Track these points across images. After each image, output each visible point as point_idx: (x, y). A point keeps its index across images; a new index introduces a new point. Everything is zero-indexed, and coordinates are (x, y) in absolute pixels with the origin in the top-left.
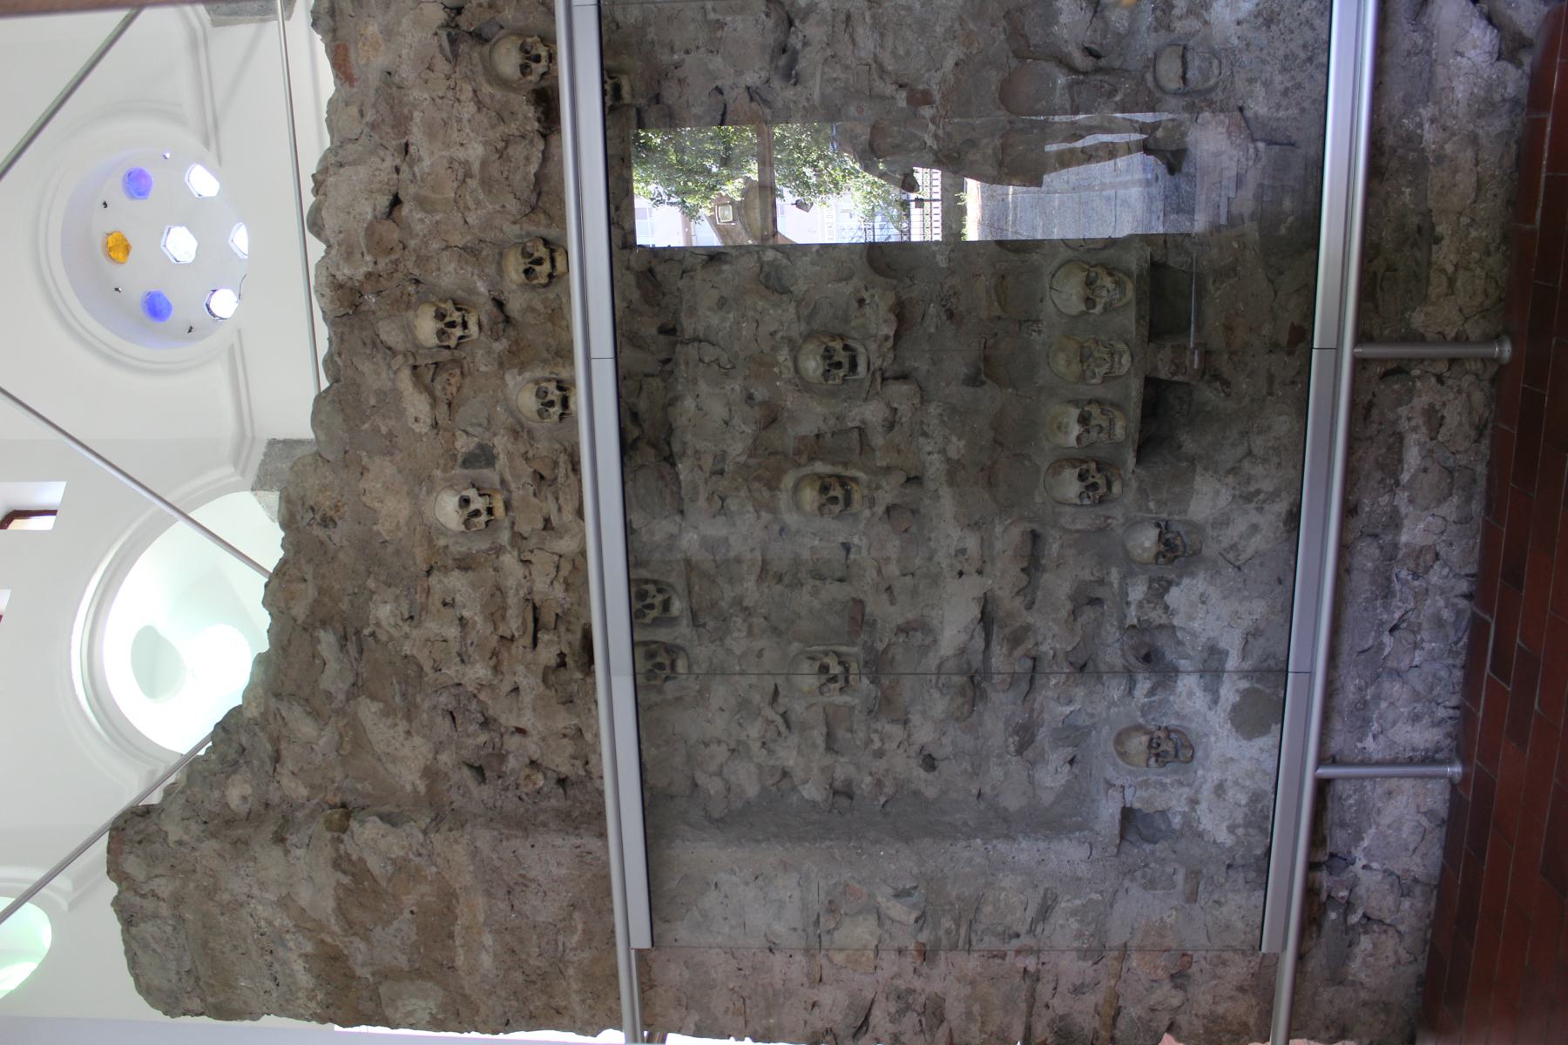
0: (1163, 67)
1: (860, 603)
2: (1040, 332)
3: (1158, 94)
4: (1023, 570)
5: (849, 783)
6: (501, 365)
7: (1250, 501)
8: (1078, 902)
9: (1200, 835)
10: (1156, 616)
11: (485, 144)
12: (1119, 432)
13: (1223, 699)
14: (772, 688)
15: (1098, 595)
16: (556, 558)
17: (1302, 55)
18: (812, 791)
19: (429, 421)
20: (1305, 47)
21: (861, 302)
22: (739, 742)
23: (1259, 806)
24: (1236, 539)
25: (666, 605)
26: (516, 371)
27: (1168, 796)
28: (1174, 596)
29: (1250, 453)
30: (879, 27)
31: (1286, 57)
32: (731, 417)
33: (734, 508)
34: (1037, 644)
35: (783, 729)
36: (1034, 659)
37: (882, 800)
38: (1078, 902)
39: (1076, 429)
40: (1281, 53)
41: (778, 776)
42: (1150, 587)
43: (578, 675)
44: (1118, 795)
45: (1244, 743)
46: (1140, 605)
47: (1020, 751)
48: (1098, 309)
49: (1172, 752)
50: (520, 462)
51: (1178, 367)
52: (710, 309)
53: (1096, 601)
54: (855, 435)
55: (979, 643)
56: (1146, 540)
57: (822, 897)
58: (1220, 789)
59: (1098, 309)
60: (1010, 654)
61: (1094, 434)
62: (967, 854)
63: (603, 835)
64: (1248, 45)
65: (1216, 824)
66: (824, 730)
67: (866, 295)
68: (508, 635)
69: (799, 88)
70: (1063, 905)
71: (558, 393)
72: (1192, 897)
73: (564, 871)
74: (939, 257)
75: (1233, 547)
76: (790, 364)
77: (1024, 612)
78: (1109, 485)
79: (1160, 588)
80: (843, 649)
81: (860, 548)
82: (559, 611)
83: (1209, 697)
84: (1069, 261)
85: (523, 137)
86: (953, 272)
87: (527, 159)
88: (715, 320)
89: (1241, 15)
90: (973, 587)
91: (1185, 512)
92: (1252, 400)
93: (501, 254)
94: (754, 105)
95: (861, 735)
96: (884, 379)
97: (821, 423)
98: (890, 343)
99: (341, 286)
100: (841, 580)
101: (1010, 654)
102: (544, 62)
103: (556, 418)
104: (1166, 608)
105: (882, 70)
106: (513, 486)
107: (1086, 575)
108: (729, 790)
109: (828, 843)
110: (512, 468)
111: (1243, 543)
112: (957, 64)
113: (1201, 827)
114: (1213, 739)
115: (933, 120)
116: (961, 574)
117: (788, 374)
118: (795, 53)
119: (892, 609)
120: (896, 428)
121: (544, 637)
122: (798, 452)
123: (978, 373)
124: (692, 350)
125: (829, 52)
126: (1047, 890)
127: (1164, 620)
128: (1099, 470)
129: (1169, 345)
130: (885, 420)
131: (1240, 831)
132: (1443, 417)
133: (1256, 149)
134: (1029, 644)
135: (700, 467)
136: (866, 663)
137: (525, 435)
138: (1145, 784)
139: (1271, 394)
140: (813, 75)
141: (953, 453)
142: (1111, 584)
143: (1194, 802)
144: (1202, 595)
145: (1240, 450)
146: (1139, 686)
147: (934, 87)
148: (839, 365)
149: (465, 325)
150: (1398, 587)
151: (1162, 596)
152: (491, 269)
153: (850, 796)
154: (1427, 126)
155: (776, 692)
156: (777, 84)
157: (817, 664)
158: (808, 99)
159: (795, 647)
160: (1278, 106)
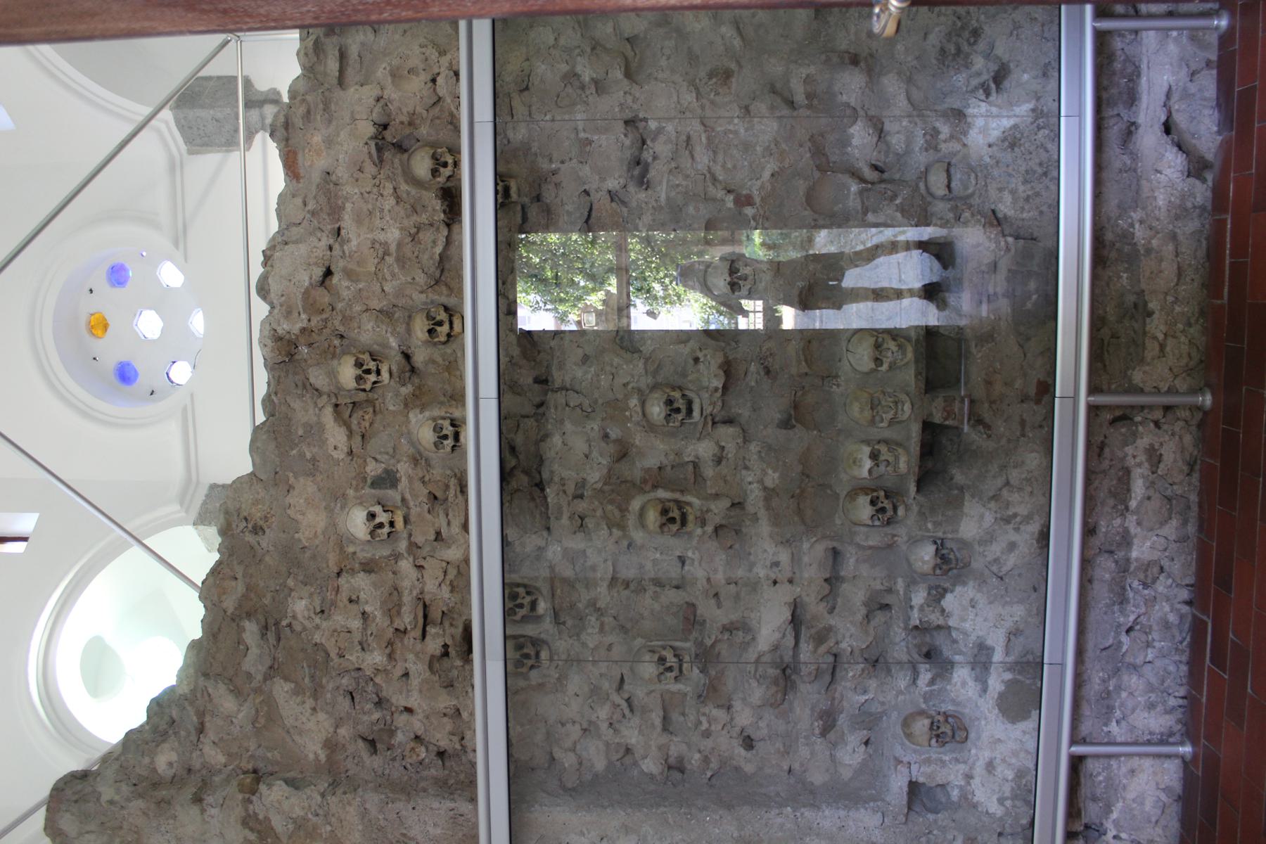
1: (692, 606)
2: (838, 386)
3: (929, 199)
5: (681, 759)
6: (406, 405)
10: (935, 618)
11: (401, 229)
13: (990, 688)
16: (444, 564)
17: (1040, 171)
18: (650, 765)
19: (346, 449)
20: (1041, 164)
21: (696, 360)
22: (590, 722)
24: (998, 554)
25: (533, 605)
26: (418, 411)
27: (947, 771)
28: (949, 601)
29: (1007, 483)
30: (712, 146)
31: (1027, 172)
32: (591, 452)
34: (837, 643)
35: (627, 712)
36: (835, 655)
37: (709, 774)
39: (868, 464)
40: (1023, 169)
41: (622, 751)
42: (929, 594)
43: (458, 663)
45: (1009, 726)
46: (921, 609)
48: (885, 367)
49: (950, 733)
52: (576, 364)
53: (886, 607)
54: (690, 468)
55: (790, 641)
58: (990, 767)
59: (885, 367)
60: (815, 651)
64: (997, 162)
66: (661, 713)
67: (700, 355)
68: (402, 628)
69: (650, 192)
73: (439, 831)
75: (996, 560)
76: (639, 409)
79: (937, 595)
82: (445, 609)
85: (431, 225)
87: (434, 242)
89: (991, 140)
90: (785, 594)
91: (957, 531)
92: (1009, 441)
93: (410, 317)
94: (614, 205)
95: (692, 718)
96: (714, 423)
97: (663, 458)
99: (280, 339)
101: (815, 651)
102: (450, 168)
103: (449, 449)
104: (943, 611)
105: (715, 180)
106: (411, 504)
108: (580, 764)
116: (775, 582)
121: (431, 630)
122: (644, 481)
123: (789, 419)
124: (560, 398)
127: (941, 622)
128: (887, 497)
130: (714, 455)
134: (831, 643)
135: (565, 492)
136: (697, 655)
138: (928, 761)
139: (1023, 435)
141: (769, 483)
143: (969, 777)
145: (1000, 482)
146: (921, 676)
148: (678, 410)
149: (378, 372)
152: (401, 329)
154: (1137, 226)
155: (622, 680)
156: (632, 189)
157: (656, 657)
159: (639, 642)
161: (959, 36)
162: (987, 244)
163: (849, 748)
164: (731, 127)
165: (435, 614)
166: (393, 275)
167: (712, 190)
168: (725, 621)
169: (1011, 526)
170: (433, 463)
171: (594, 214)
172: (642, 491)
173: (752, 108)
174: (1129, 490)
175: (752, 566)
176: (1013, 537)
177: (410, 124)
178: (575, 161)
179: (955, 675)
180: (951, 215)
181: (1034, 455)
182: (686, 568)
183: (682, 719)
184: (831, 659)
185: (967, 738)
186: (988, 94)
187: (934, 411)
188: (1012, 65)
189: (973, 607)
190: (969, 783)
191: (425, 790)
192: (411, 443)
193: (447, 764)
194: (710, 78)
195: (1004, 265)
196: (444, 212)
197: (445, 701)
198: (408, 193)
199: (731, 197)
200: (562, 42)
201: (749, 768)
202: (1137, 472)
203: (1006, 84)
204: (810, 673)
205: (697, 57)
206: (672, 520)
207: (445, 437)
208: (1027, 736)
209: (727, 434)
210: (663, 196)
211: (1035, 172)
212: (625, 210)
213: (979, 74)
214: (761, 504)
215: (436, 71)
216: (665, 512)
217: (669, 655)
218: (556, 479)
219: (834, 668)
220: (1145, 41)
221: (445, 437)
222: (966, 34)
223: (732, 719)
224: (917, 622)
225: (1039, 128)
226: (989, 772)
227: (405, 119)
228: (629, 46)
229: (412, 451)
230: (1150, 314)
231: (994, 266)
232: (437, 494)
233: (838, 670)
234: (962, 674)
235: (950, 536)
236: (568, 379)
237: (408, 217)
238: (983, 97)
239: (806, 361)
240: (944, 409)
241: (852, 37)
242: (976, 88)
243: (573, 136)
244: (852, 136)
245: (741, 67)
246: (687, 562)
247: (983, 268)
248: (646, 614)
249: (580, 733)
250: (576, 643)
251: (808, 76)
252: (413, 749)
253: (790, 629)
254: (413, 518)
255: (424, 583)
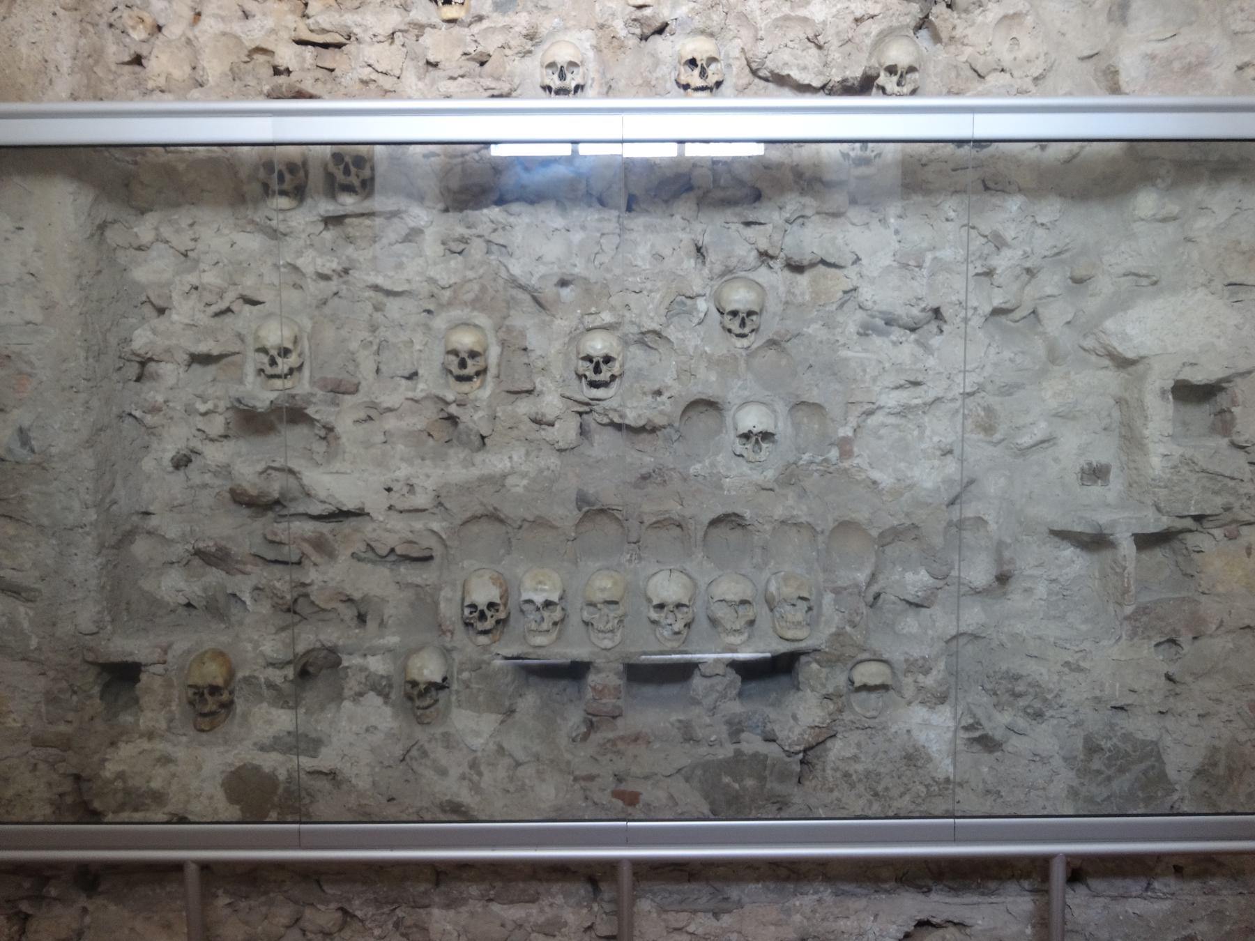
0: (874, 667)
1: (355, 390)
2: (630, 561)
3: (850, 665)
4: (392, 550)
5: (155, 377)
6: (602, 27)
7: (471, 767)
8: (26, 625)
9: (113, 744)
10: (352, 685)
11: (824, 23)
12: (539, 640)
13: (266, 755)
14: (260, 299)
15: (369, 623)
16: (397, 73)
17: (880, 788)
18: (142, 340)
20: (887, 789)
21: (659, 393)
22: (197, 261)
23: (148, 801)
24: (432, 756)
25: (348, 189)
26: (594, 42)
27: (156, 708)
28: (373, 699)
29: (518, 764)
30: (905, 411)
31: (879, 774)
32: (545, 264)
33: (452, 263)
34: (315, 565)
35: (215, 309)
36: (299, 563)
37: (138, 414)
38: (26, 625)
39: (539, 599)
40: (882, 770)
41: (160, 303)
42: (382, 677)
43: (266, 88)
44: (156, 657)
45: (219, 780)
46: (363, 669)
47: (198, 553)
48: (654, 615)
49: (206, 710)
50: (499, 39)
51: (600, 692)
52: (653, 246)
53: (361, 619)
54: (528, 387)
55: (316, 509)
56: (429, 668)
57: (17, 349)
58: (166, 760)
59: (654, 615)
60: (305, 540)
61: (537, 616)
62: (77, 505)
63: (74, 97)
64: (890, 741)
65: (122, 761)
66: (215, 352)
67: (664, 398)
68: (310, 11)
69: (855, 337)
70: (22, 609)
71: (573, 85)
72: (38, 742)
73: (24, 50)
74: (698, 466)
75: (425, 754)
76: (597, 324)
77: (349, 552)
78: (485, 632)
79: (381, 687)
80: (306, 372)
81: (414, 389)
82: (337, 72)
83: (267, 742)
84: (695, 585)
85: (826, 65)
86: (685, 480)
87: (805, 68)
88: (643, 250)
89: (915, 733)
90: (375, 503)
91: (460, 706)
92: (568, 763)
93: (712, 35)
94: (840, 294)
95: (210, 391)
96: (580, 414)
97: (539, 352)
98: (617, 420)
100: (378, 371)
101: (305, 540)
102: (897, 89)
103: (547, 82)
104: (361, 694)
105: (870, 413)
106: (476, 28)
107: (389, 611)
108: (139, 248)
109: (82, 354)
110: (492, 30)
111: (429, 763)
112: (874, 482)
113: (122, 745)
114: (222, 749)
115: (826, 460)
116: (389, 490)
117: (589, 321)
118: (887, 334)
119: (349, 421)
120: (535, 426)
121: (309, 52)
122: (509, 330)
123: (589, 503)
124: (612, 226)
125: (887, 365)
126: (40, 591)
127: (347, 692)
128: (498, 622)
129: (619, 682)
130: (543, 415)
131: (119, 784)
132: (554, 936)
133: (797, 753)
134: (315, 557)
135: (495, 230)
136: (293, 397)
137: (528, 47)
138: (169, 684)
139: (576, 779)
140: (865, 350)
141: (510, 481)
142: (382, 637)
143: (150, 735)
144: (376, 728)
145: (520, 755)
146: (278, 672)
147: (856, 461)
148: (597, 370)
150: (386, 910)
151: (373, 688)
152: (698, 23)
153: (138, 379)
154: (816, 897)
155: (254, 303)
156: (860, 315)
157: (290, 346)
158: (844, 345)
159: (307, 324)
160: (836, 770)
161: (1036, 697)
162: (797, 730)
163: (182, 585)
164: (928, 433)
165: (329, 58)
166: (766, 12)
167: (857, 411)
168: (339, 429)
169: (467, 770)
170: (528, 60)
171: (833, 270)
172: (498, 329)
173: (949, 457)
174: (512, 902)
175: (409, 461)
176: (454, 772)
177: (952, 38)
178: (897, 246)
179: (281, 711)
180: (831, 690)
181: (553, 792)
182: (404, 382)
183: (209, 378)
184: (295, 558)
185: (202, 731)
186: (966, 729)
187: (603, 675)
188: (998, 754)
189: (367, 730)
190: (141, 736)
191: (83, 32)
192: (554, 31)
193: (127, 68)
194: (984, 409)
195: (772, 750)
196: (845, 80)
197: (214, 68)
198: (867, 35)
199: (850, 434)
200: (1040, 232)
201: (148, 464)
202: (534, 909)
203: (977, 747)
204: (276, 534)
205: (1010, 394)
206: (463, 364)
207: (562, 77)
208: (206, 802)
209: (566, 431)
210: (850, 354)
211: (878, 783)
212: (834, 307)
213: (989, 718)
214: (486, 471)
215: (1016, 73)
216: (473, 354)
217: (293, 360)
218: (511, 219)
219: (285, 563)
220: (1020, 899)
221: (562, 77)
222: (1038, 704)
223: (212, 440)
224: (345, 663)
225: (927, 786)
226: (159, 760)
227: (958, 33)
228: (1025, 313)
229: (543, 31)
230: (716, 915)
231: (770, 739)
232: (487, 65)
233: (281, 567)
234: (283, 720)
235: (454, 698)
236: (634, 236)
237: (838, 34)
238: (963, 723)
239: (658, 522)
240: (605, 687)
241: (1028, 572)
242: (974, 716)
243: (925, 245)
244: (916, 573)
245: (996, 444)
246: (409, 383)
247: (769, 727)
248: (343, 332)
249: (182, 249)
250: (301, 243)
251: (986, 522)
252: (143, 21)
253: (332, 508)
254: (456, 29)
255: (372, 44)
